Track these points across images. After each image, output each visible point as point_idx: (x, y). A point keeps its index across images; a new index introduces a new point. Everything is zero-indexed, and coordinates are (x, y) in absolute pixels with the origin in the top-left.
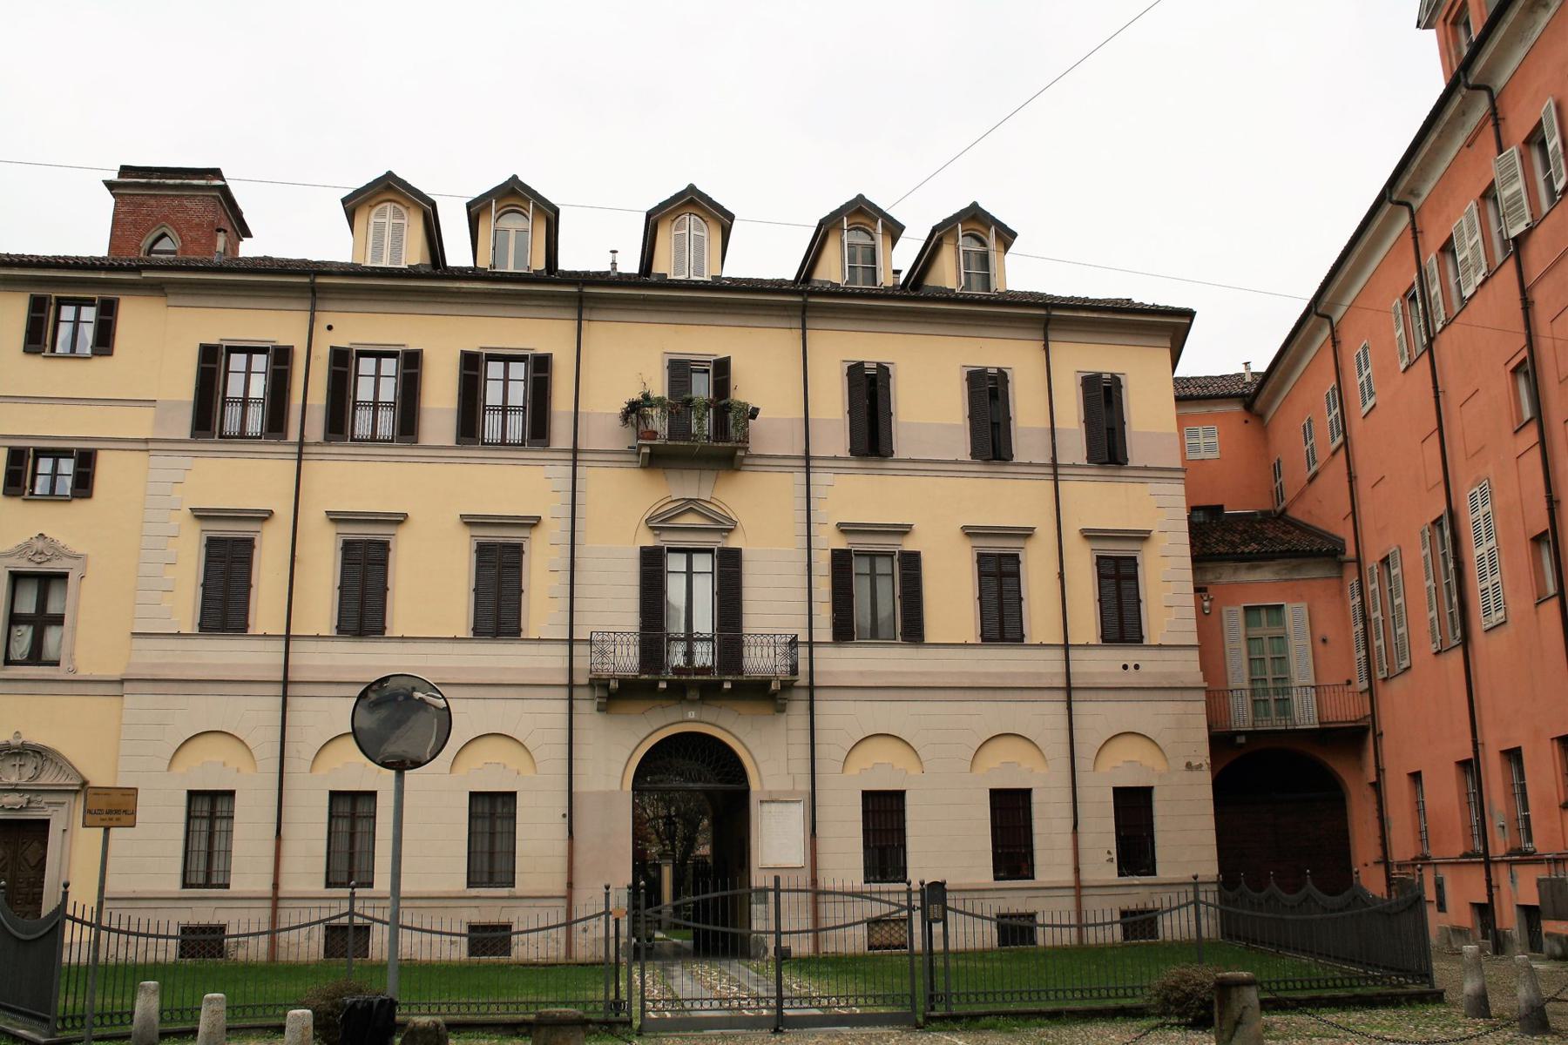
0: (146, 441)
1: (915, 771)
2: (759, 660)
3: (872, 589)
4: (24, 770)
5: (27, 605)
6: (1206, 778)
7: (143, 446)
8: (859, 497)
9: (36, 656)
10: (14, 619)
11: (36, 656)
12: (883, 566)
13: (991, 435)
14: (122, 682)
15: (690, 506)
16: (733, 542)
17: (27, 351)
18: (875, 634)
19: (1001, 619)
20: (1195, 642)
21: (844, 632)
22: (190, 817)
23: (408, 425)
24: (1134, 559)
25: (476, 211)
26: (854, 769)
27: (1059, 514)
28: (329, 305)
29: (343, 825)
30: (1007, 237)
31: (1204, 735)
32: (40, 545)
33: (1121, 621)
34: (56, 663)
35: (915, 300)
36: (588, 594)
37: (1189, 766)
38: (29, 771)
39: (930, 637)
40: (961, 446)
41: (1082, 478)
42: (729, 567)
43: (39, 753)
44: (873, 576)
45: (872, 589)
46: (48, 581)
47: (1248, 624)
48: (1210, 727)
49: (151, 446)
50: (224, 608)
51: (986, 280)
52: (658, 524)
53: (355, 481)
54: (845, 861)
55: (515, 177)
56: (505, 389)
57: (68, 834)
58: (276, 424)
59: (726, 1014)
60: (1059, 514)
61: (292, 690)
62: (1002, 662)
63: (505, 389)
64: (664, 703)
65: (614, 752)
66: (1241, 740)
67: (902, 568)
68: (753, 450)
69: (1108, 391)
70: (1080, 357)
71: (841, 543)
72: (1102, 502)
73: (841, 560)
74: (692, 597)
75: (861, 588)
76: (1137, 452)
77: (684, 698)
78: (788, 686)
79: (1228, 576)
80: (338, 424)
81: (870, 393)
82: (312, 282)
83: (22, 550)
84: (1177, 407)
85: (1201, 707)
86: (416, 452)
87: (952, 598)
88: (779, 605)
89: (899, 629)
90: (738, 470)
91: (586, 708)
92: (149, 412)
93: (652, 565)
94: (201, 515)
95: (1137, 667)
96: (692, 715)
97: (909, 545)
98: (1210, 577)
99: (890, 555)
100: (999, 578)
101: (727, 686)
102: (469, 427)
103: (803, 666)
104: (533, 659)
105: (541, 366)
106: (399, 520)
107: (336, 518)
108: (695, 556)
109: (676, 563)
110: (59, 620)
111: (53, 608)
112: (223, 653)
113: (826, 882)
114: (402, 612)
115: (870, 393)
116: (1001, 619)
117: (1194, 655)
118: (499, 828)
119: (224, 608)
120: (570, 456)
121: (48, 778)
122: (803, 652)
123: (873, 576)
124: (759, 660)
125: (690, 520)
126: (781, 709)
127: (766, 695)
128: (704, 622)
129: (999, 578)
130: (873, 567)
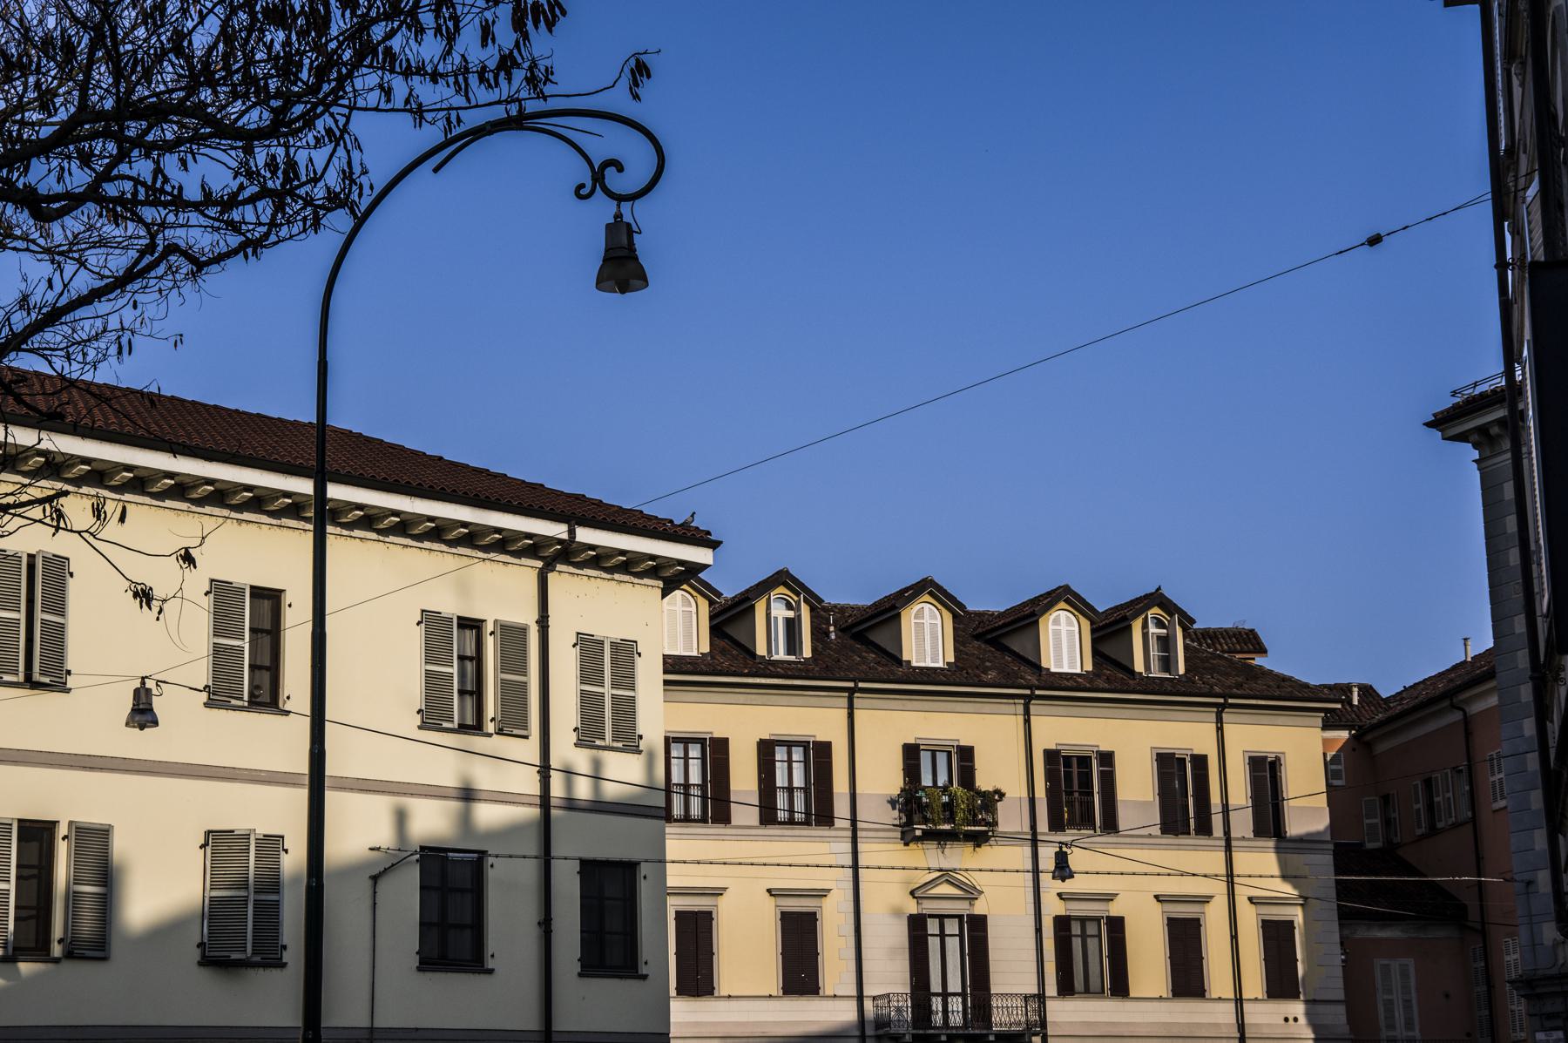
16: (979, 908)
17: (602, 282)
18: (1087, 992)
19: (1187, 978)
21: (1066, 988)
39: (1132, 994)
41: (1251, 849)
63: (792, 773)
73: (1062, 923)
86: (833, 833)
97: (1114, 910)
99: (1097, 920)
100: (1184, 938)
105: (819, 754)
108: (946, 921)
116: (1187, 978)
117: (1342, 1009)
129: (1184, 938)
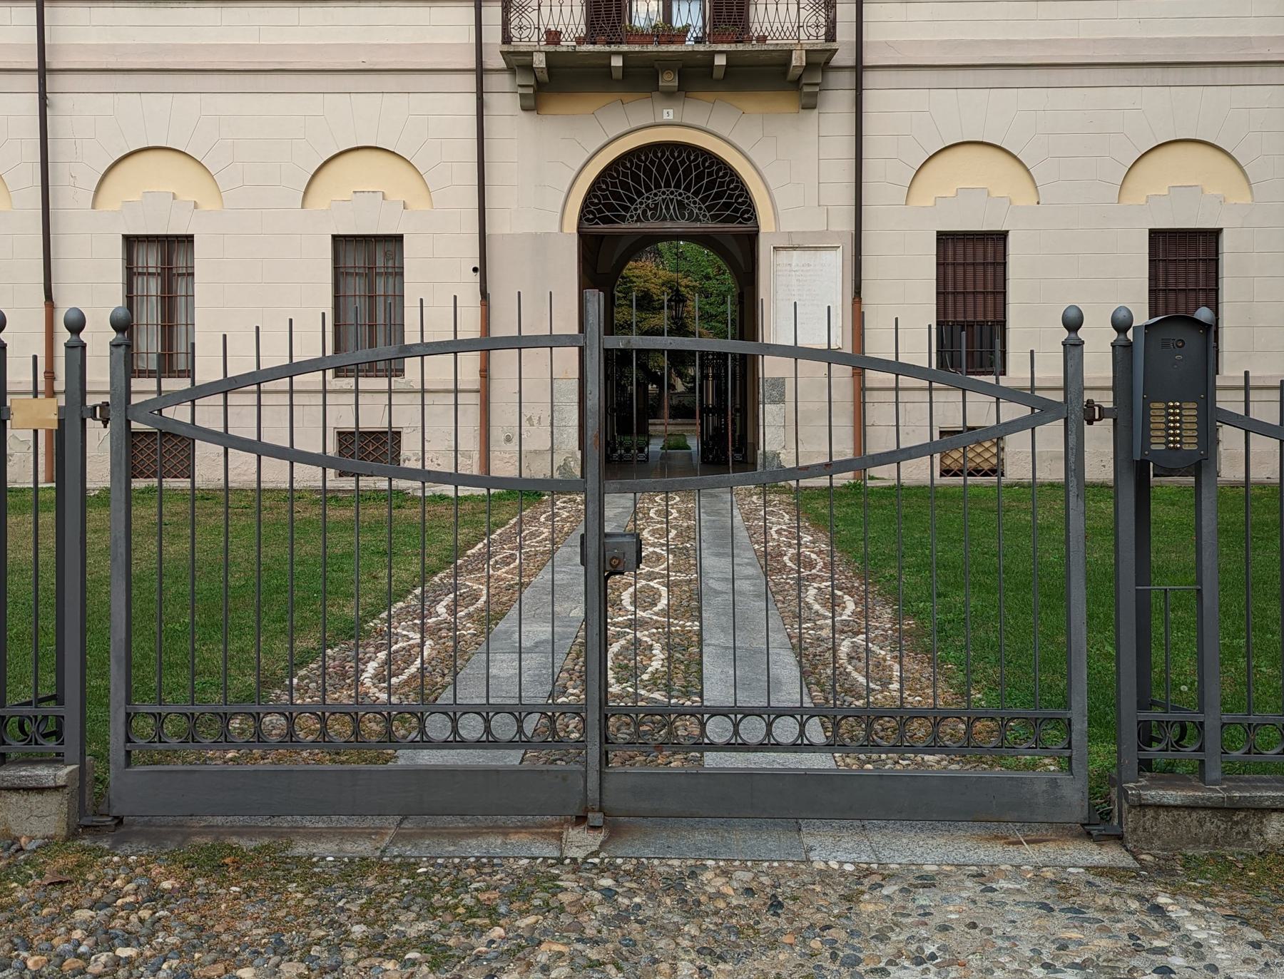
22: (131, 273)
26: (927, 193)
29: (356, 286)
54: (907, 315)
59: (512, 758)
61: (53, 82)
64: (627, 97)
65: (551, 167)
77: (657, 88)
78: (820, 63)
96: (668, 114)
101: (720, 61)
103: (845, 34)
118: (380, 290)
127: (786, 79)
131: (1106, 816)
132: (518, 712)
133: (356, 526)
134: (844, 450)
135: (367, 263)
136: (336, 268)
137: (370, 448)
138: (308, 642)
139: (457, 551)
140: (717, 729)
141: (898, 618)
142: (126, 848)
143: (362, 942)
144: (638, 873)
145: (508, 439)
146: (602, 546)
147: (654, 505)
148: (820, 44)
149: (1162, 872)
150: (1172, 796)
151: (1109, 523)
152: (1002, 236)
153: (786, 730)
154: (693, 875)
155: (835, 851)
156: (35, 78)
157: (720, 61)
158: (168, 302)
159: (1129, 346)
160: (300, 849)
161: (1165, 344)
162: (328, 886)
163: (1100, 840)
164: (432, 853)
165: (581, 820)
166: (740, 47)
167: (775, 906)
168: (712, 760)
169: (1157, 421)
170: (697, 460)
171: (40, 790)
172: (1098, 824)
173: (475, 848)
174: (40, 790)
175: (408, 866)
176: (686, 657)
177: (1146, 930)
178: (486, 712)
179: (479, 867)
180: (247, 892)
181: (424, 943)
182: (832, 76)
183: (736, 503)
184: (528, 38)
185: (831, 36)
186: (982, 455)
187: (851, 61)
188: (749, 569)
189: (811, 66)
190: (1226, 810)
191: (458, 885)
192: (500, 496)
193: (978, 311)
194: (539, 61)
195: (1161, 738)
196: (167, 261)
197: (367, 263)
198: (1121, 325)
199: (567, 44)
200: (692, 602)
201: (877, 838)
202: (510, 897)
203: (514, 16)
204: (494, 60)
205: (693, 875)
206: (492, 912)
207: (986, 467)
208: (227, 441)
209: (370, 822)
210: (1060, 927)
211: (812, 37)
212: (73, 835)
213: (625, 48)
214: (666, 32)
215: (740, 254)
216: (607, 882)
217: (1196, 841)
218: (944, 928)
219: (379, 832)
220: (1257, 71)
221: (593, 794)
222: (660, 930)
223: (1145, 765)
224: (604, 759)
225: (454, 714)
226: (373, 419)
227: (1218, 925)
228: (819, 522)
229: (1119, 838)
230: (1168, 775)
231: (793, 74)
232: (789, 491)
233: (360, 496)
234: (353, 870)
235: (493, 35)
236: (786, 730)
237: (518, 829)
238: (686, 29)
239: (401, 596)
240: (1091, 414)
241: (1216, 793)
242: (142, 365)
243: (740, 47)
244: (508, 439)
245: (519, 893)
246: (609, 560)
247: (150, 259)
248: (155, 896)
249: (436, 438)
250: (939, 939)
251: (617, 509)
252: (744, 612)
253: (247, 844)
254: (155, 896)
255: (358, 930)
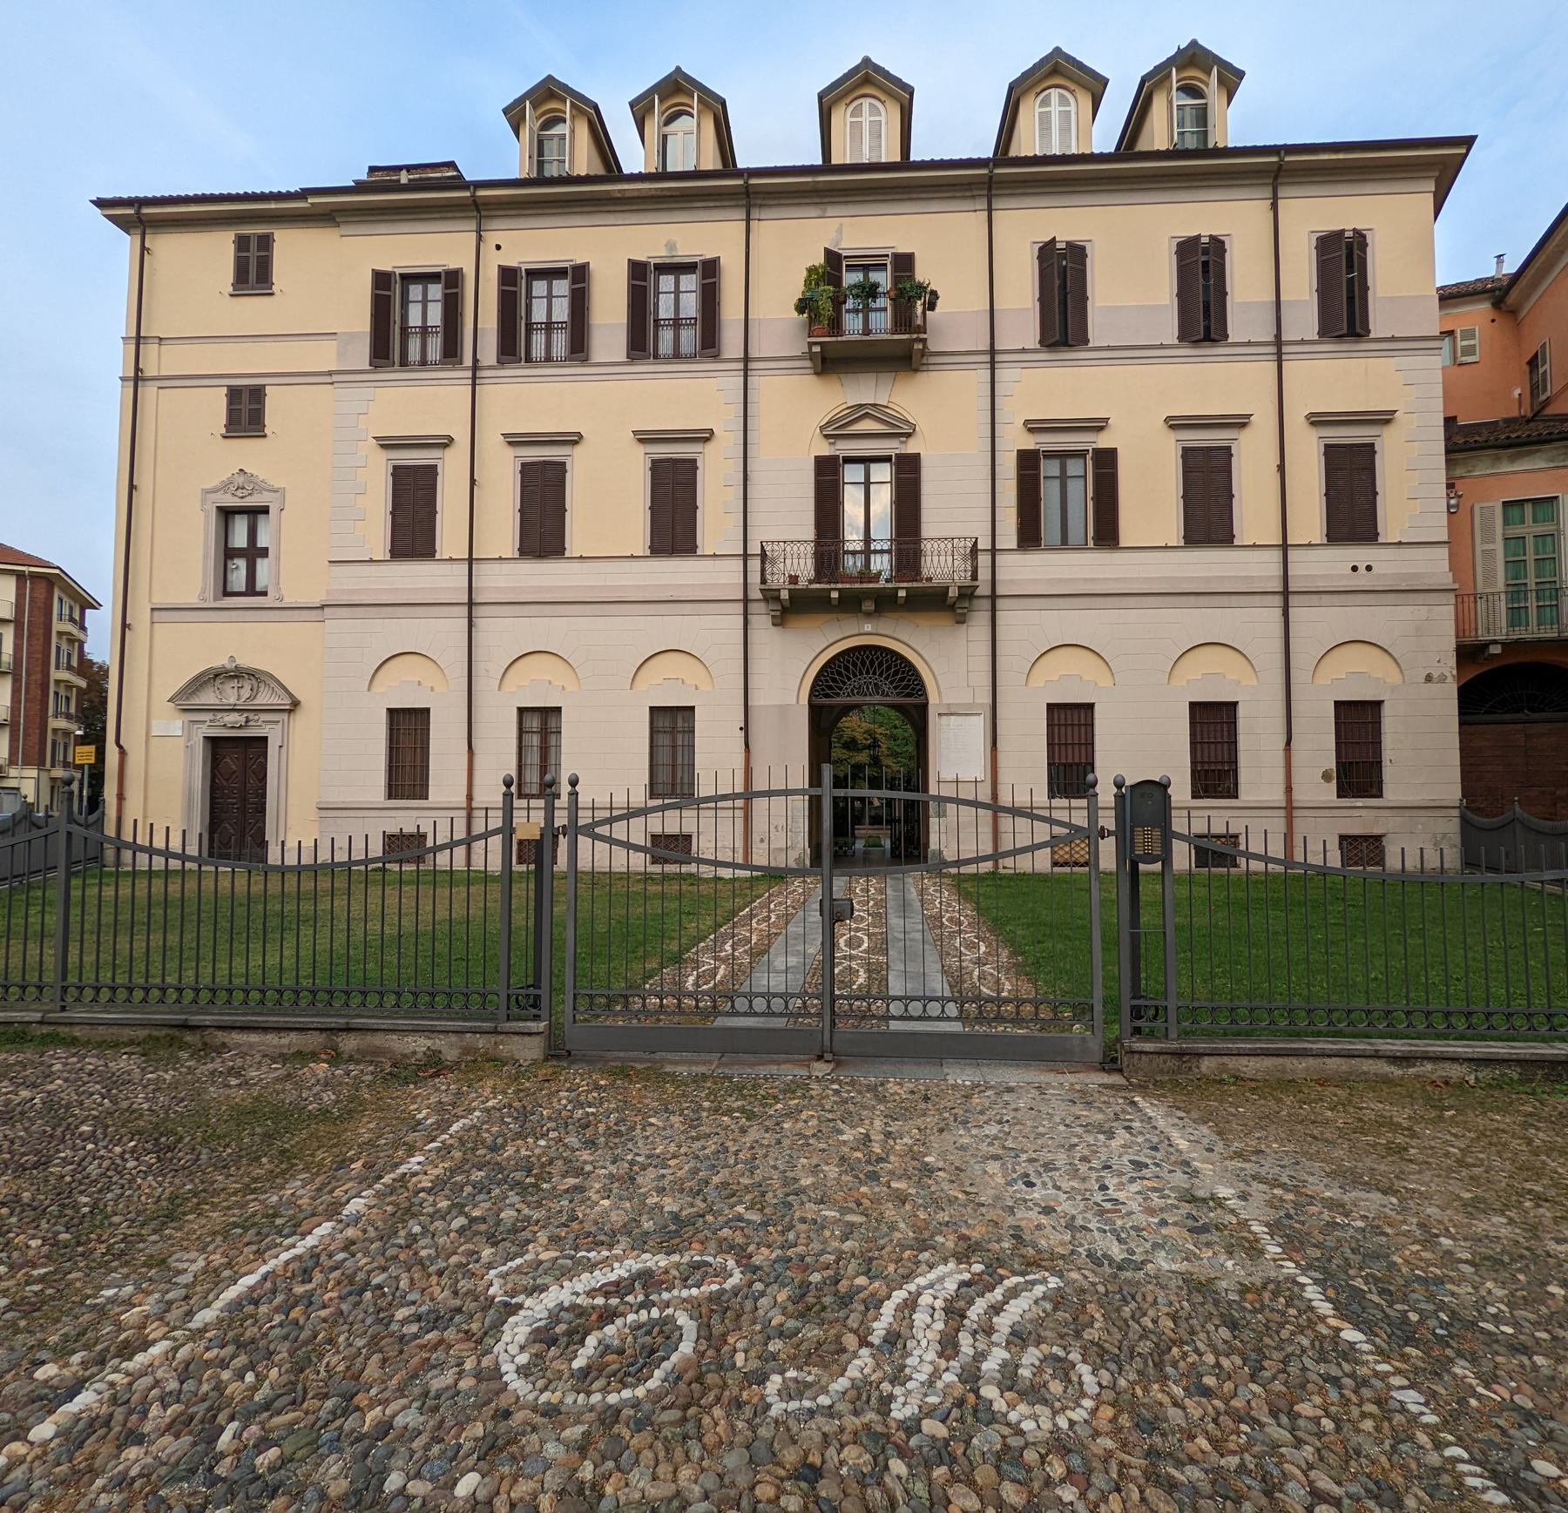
0: (330, 373)
1: (1105, 682)
2: (940, 565)
3: (1067, 489)
4: (242, 691)
5: (240, 539)
6: (1452, 689)
7: (328, 379)
8: (1048, 390)
9: (251, 590)
10: (229, 553)
11: (251, 590)
12: (1074, 467)
13: (1202, 309)
14: (322, 607)
15: (862, 411)
16: (911, 448)
19: (1208, 512)
20: (1445, 538)
22: (521, 731)
23: (579, 347)
24: (1372, 445)
25: (641, 110)
26: (1038, 680)
27: (1276, 398)
28: (496, 224)
29: (664, 740)
30: (1231, 79)
31: (1451, 644)
32: (240, 480)
33: (1352, 507)
34: (264, 594)
35: (1128, 170)
36: (763, 506)
37: (1429, 678)
38: (246, 693)
40: (1168, 327)
42: (908, 472)
43: (253, 676)
44: (1063, 478)
45: (1067, 489)
46: (256, 513)
47: (1506, 522)
48: (1459, 632)
49: (335, 378)
50: (413, 533)
51: (1205, 135)
52: (835, 430)
53: (530, 400)
54: (1027, 776)
55: (678, 69)
56: (677, 299)
57: (284, 750)
58: (451, 352)
60: (1276, 398)
61: (477, 611)
62: (1208, 564)
65: (791, 663)
66: (1495, 650)
67: (1096, 467)
68: (932, 347)
69: (1350, 247)
70: (1313, 213)
71: (1030, 443)
72: (1334, 380)
73: (1028, 462)
74: (868, 509)
75: (1049, 493)
76: (1380, 322)
78: (968, 594)
79: (1482, 468)
80: (511, 348)
81: (1063, 275)
82: (473, 196)
83: (224, 487)
84: (1441, 307)
85: (1449, 611)
87: (1152, 498)
88: (963, 509)
89: (1091, 533)
90: (917, 370)
91: (761, 621)
92: (331, 346)
93: (828, 476)
94: (388, 444)
95: (1369, 568)
96: (868, 628)
97: (1104, 441)
98: (1459, 472)
99: (1081, 454)
101: (902, 593)
102: (640, 344)
103: (984, 574)
104: (712, 571)
106: (574, 440)
107: (515, 441)
109: (853, 473)
110: (264, 552)
111: (262, 542)
112: (413, 576)
113: (1005, 799)
114: (579, 532)
115: (1063, 275)
116: (1208, 512)
119: (413, 533)
120: (741, 366)
121: (265, 698)
122: (984, 560)
123: (1063, 478)
124: (940, 565)
125: (867, 426)
126: (961, 620)
127: (946, 604)
128: (883, 530)
130: (1063, 469)
131: (1114, 1060)
132: (786, 996)
133: (663, 896)
134: (987, 848)
135: (671, 726)
136: (651, 728)
137: (671, 847)
138: (652, 964)
139: (734, 913)
140: (896, 1008)
141: (1013, 954)
142: (575, 1066)
143: (709, 1109)
144: (852, 1083)
145: (762, 841)
146: (832, 906)
147: (859, 885)
148: (968, 582)
149: (1142, 1088)
150: (1149, 1047)
151: (1159, 899)
152: (1091, 706)
153: (934, 1009)
154: (882, 1084)
155: (961, 1076)
156: (466, 609)
157: (902, 593)
158: (544, 750)
159: (1123, 796)
160: (668, 1069)
161: (1142, 796)
162: (687, 1085)
163: (1110, 1071)
164: (738, 1073)
165: (820, 1058)
166: (915, 585)
167: (926, 1099)
168: (895, 1025)
169: (1139, 839)
170: (888, 854)
171: (530, 1034)
172: (1110, 1063)
173: (762, 1071)
174: (530, 1034)
175: (730, 1079)
176: (878, 973)
177: (1124, 1111)
178: (769, 996)
179: (766, 1079)
180: (645, 1087)
181: (742, 1110)
182: (976, 602)
183: (913, 882)
184: (778, 580)
185: (974, 577)
186: (1081, 851)
187: (988, 592)
188: (915, 923)
189: (961, 596)
190: (1179, 1054)
191: (755, 1087)
192: (757, 878)
193: (1073, 756)
194: (785, 595)
195: (1143, 1015)
196: (544, 724)
197: (671, 726)
198: (1119, 784)
199: (802, 584)
200: (882, 945)
201: (985, 1069)
202: (785, 1092)
203: (768, 566)
204: (755, 594)
205: (882, 1084)
206: (775, 1097)
207: (1082, 860)
208: (628, 846)
209: (707, 1057)
210: (1079, 1110)
211: (962, 577)
212: (546, 1059)
213: (840, 586)
214: (866, 575)
215: (916, 716)
216: (836, 1087)
217: (1162, 1072)
218: (1016, 1110)
219: (710, 1062)
220: (1257, 597)
221: (827, 1043)
222: (864, 1107)
223: (1137, 1031)
224: (833, 1024)
225: (750, 996)
226: (672, 828)
227: (1163, 1110)
228: (963, 896)
229: (1120, 1071)
230: (1151, 1036)
231: (949, 601)
232: (949, 876)
233: (665, 877)
234: (699, 1079)
235: (755, 578)
236: (934, 1009)
237: (785, 1062)
238: (880, 573)
239: (703, 939)
240: (1102, 833)
241: (1175, 1045)
242: (527, 791)
243: (915, 585)
244: (762, 841)
245: (789, 1090)
246: (835, 913)
247: (534, 723)
248: (598, 1088)
249: (715, 837)
250: (1012, 1114)
251: (839, 884)
252: (915, 945)
253: (639, 1066)
254: (598, 1088)
255: (706, 1104)
